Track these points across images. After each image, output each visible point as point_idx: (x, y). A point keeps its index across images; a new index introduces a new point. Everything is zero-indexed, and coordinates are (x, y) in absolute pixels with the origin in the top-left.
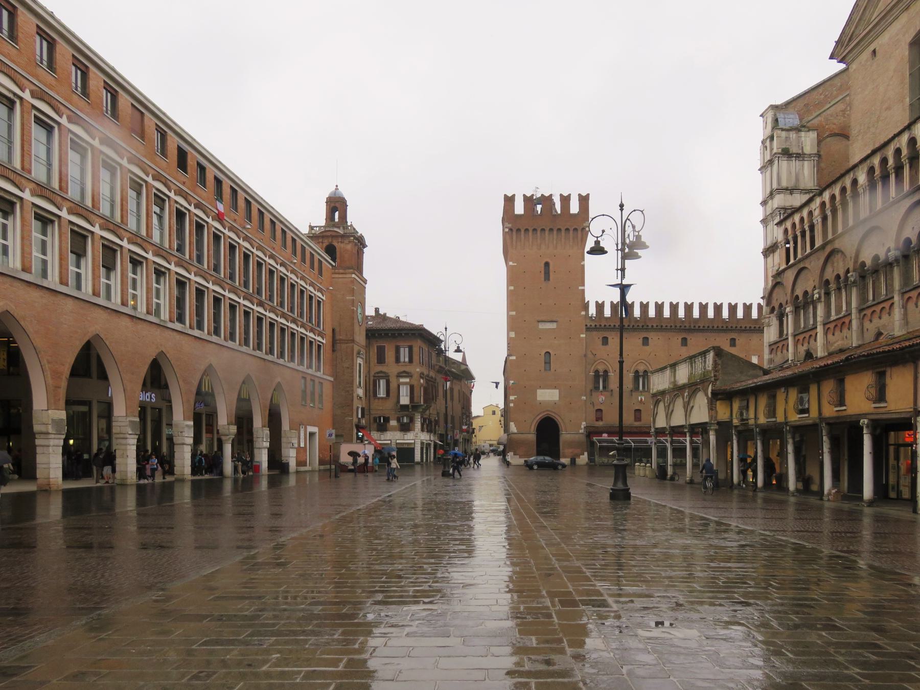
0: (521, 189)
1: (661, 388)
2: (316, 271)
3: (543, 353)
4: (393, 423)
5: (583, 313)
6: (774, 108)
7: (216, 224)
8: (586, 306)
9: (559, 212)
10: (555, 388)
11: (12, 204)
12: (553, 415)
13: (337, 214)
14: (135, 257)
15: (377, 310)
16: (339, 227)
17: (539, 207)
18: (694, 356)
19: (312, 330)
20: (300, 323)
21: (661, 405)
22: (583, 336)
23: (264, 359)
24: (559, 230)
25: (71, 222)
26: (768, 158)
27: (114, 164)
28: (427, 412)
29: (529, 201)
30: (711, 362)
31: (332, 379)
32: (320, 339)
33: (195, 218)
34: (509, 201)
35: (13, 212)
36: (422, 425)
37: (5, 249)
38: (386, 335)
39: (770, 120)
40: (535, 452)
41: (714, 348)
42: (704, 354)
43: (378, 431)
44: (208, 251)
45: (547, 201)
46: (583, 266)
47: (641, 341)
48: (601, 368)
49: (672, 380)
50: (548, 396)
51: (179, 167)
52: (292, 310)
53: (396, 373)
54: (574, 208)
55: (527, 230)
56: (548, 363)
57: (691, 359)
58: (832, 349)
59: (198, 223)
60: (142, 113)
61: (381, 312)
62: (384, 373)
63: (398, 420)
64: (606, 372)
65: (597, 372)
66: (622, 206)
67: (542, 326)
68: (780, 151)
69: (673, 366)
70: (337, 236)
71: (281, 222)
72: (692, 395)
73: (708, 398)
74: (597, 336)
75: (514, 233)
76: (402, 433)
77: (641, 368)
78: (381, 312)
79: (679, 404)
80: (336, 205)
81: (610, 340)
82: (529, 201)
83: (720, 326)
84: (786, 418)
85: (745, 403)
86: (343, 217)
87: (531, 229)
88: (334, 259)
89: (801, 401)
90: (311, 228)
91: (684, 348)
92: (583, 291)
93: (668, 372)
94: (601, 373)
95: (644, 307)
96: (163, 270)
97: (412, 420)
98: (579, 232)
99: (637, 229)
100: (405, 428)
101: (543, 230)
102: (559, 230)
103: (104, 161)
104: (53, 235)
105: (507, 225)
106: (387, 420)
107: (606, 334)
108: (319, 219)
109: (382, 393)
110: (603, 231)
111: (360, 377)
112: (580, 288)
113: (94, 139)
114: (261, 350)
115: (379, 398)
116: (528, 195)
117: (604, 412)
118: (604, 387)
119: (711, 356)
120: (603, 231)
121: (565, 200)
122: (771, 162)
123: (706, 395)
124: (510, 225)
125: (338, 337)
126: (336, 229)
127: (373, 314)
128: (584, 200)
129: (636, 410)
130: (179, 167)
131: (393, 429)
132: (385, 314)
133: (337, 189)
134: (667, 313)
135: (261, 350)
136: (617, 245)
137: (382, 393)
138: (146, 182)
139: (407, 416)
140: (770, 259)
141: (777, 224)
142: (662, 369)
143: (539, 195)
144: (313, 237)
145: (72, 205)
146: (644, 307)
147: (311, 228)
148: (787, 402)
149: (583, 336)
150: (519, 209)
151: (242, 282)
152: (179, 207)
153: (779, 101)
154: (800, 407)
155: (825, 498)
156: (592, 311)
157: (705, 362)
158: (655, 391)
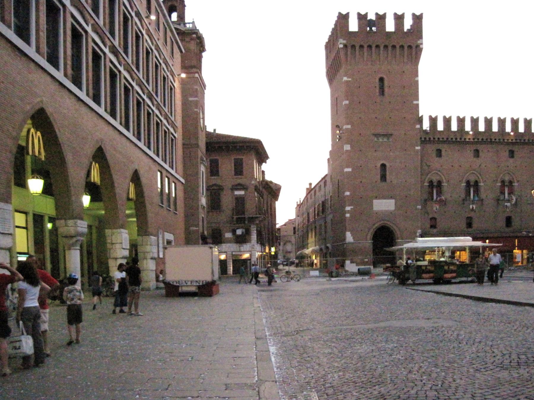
3: (379, 165)
5: (418, 126)
8: (420, 120)
10: (391, 198)
12: (389, 224)
22: (418, 148)
24: (394, 47)
38: (220, 148)
40: (132, 238)
46: (418, 81)
47: (507, 154)
48: (435, 179)
50: (384, 205)
53: (230, 186)
55: (361, 47)
56: (383, 178)
63: (234, 232)
64: (440, 183)
65: (431, 182)
74: (431, 149)
76: (238, 245)
77: (472, 179)
81: (443, 153)
83: (485, 138)
85: (88, 180)
87: (366, 46)
91: (511, 160)
92: (417, 105)
94: (435, 184)
95: (433, 121)
97: (248, 232)
98: (414, 50)
100: (241, 240)
101: (377, 46)
102: (370, 47)
107: (440, 146)
112: (415, 102)
117: (438, 221)
124: (345, 42)
128: (418, 19)
131: (229, 241)
134: (440, 127)
146: (433, 121)
149: (418, 148)
150: (353, 26)
156: (426, 125)
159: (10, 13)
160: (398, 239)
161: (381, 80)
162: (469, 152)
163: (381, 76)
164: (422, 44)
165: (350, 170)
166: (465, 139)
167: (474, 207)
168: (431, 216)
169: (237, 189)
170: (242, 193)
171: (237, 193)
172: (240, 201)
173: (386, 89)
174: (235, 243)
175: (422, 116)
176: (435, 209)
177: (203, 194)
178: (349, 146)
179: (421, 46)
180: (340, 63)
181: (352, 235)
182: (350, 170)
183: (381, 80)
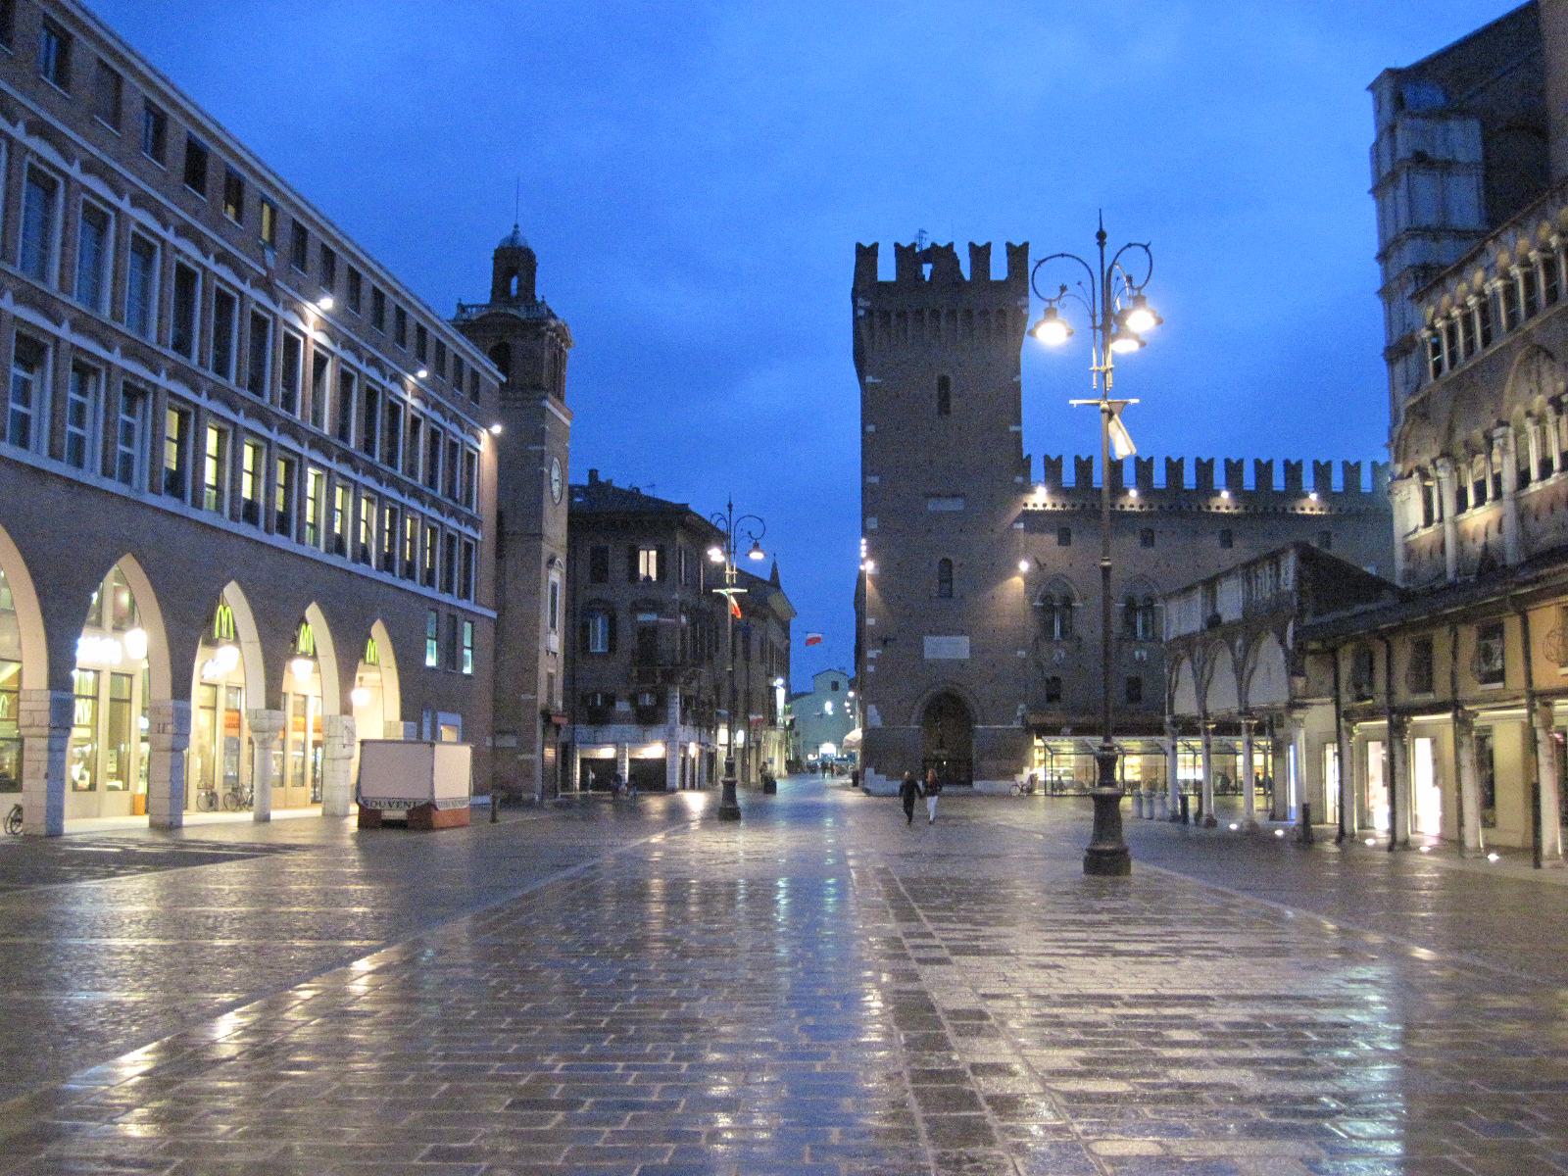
0: (889, 233)
1: (1184, 630)
2: (466, 394)
4: (623, 707)
6: (1393, 73)
7: (260, 296)
9: (967, 276)
11: (43, 349)
13: (514, 281)
14: (84, 359)
15: (593, 474)
16: (518, 308)
17: (927, 269)
18: (1255, 562)
19: (453, 513)
20: (427, 499)
21: (1186, 665)
23: (350, 573)
25: (124, 371)
26: (1386, 169)
27: (53, 175)
28: (694, 684)
29: (906, 256)
30: (1291, 575)
31: (493, 615)
32: (469, 531)
33: (216, 283)
34: (866, 256)
35: (42, 363)
36: (684, 711)
37: (23, 422)
39: (1387, 96)
41: (1296, 545)
42: (1274, 558)
43: (591, 722)
44: (240, 350)
45: (943, 255)
49: (1209, 613)
51: (397, 340)
52: (368, 448)
54: (999, 270)
57: (1248, 570)
58: (1536, 548)
59: (220, 293)
60: (118, 78)
61: (602, 478)
62: (606, 602)
63: (633, 699)
64: (1067, 602)
66: (1101, 236)
67: (932, 505)
68: (1409, 155)
69: (1211, 584)
70: (514, 324)
71: (188, 117)
72: (1253, 639)
73: (1287, 652)
75: (876, 320)
78: (602, 478)
79: (1224, 661)
80: (514, 262)
82: (906, 256)
84: (80, 697)
86: (528, 286)
88: (504, 369)
89: (1486, 655)
90: (462, 308)
92: (1018, 434)
93: (1198, 597)
96: (142, 386)
97: (662, 701)
99: (1136, 284)
103: (32, 168)
104: (97, 394)
105: (861, 302)
106: (610, 700)
108: (479, 291)
109: (599, 647)
110: (1063, 289)
111: (553, 612)
112: (1013, 428)
113: (71, 164)
114: (413, 578)
115: (593, 655)
116: (905, 244)
118: (1063, 632)
119: (1290, 563)
120: (1063, 289)
121: (980, 254)
122: (1393, 176)
123: (1282, 642)
124: (868, 304)
125: (508, 528)
126: (512, 311)
127: (585, 482)
128: (1018, 255)
129: (1129, 681)
130: (397, 340)
131: (623, 719)
132: (609, 482)
133: (515, 232)
135: (413, 578)
136: (1093, 317)
137: (599, 647)
138: (117, 210)
139: (651, 692)
140: (1399, 368)
141: (1411, 298)
142: (1187, 590)
143: (927, 245)
144: (468, 327)
145: (76, 315)
147: (462, 308)
148: (1455, 658)
150: (887, 270)
151: (246, 378)
152: (181, 259)
153: (1406, 60)
154: (1485, 668)
155: (1545, 864)
157: (1278, 575)
158: (1171, 637)
159: (20, 175)
160: (976, 722)
161: (944, 383)
162: (1132, 542)
163: (945, 372)
164: (1027, 306)
165: (1136, 401)
166: (1122, 506)
167: (1144, 654)
168: (1049, 675)
169: (642, 610)
170: (653, 617)
171: (642, 617)
172: (648, 634)
173: (954, 402)
174: (638, 723)
175: (1029, 456)
176: (1056, 657)
177: (553, 625)
178: (875, 520)
179: (1024, 311)
180: (1269, 1073)
181: (880, 711)
182: (1136, 401)
183: (944, 383)
